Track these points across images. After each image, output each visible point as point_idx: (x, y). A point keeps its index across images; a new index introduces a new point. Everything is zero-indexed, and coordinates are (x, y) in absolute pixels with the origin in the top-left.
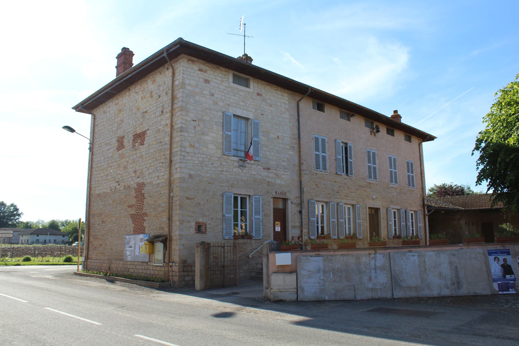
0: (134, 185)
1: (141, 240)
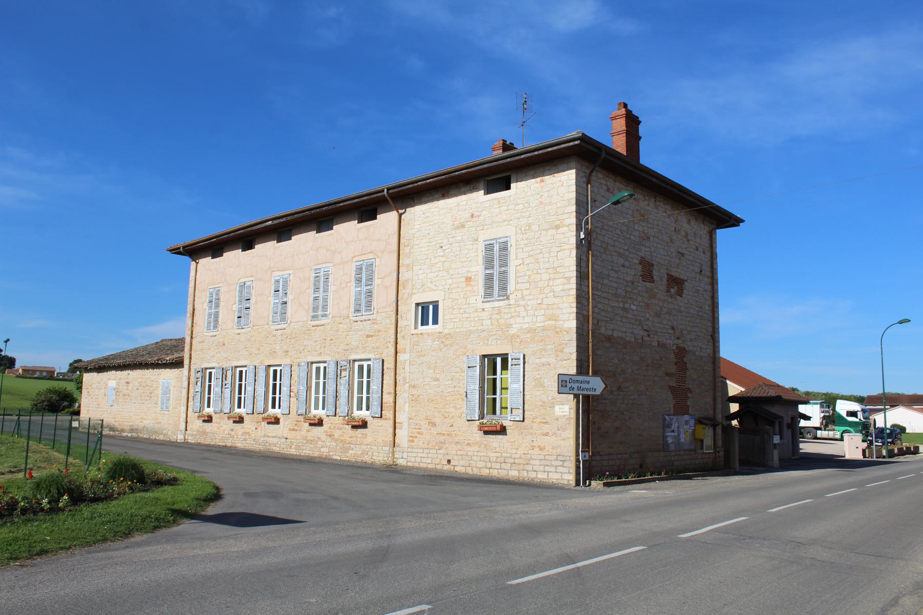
0: (672, 345)
1: (687, 422)
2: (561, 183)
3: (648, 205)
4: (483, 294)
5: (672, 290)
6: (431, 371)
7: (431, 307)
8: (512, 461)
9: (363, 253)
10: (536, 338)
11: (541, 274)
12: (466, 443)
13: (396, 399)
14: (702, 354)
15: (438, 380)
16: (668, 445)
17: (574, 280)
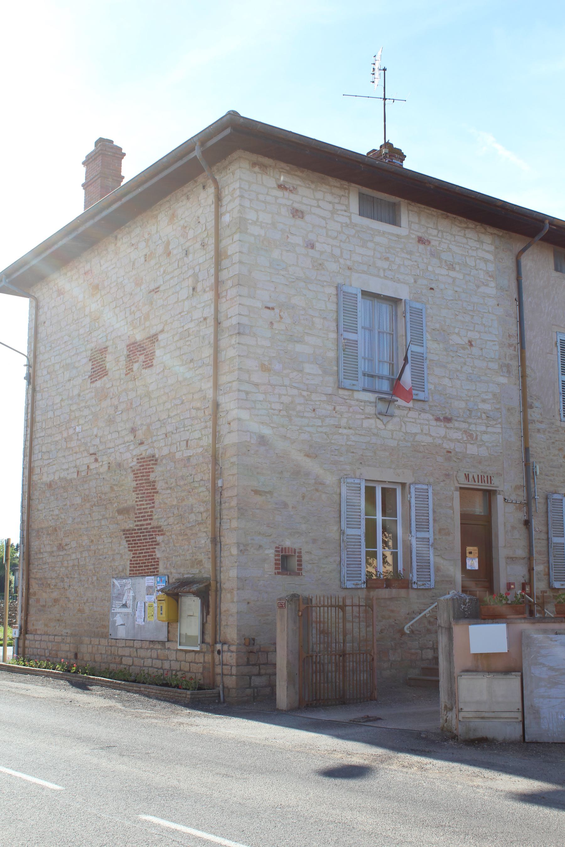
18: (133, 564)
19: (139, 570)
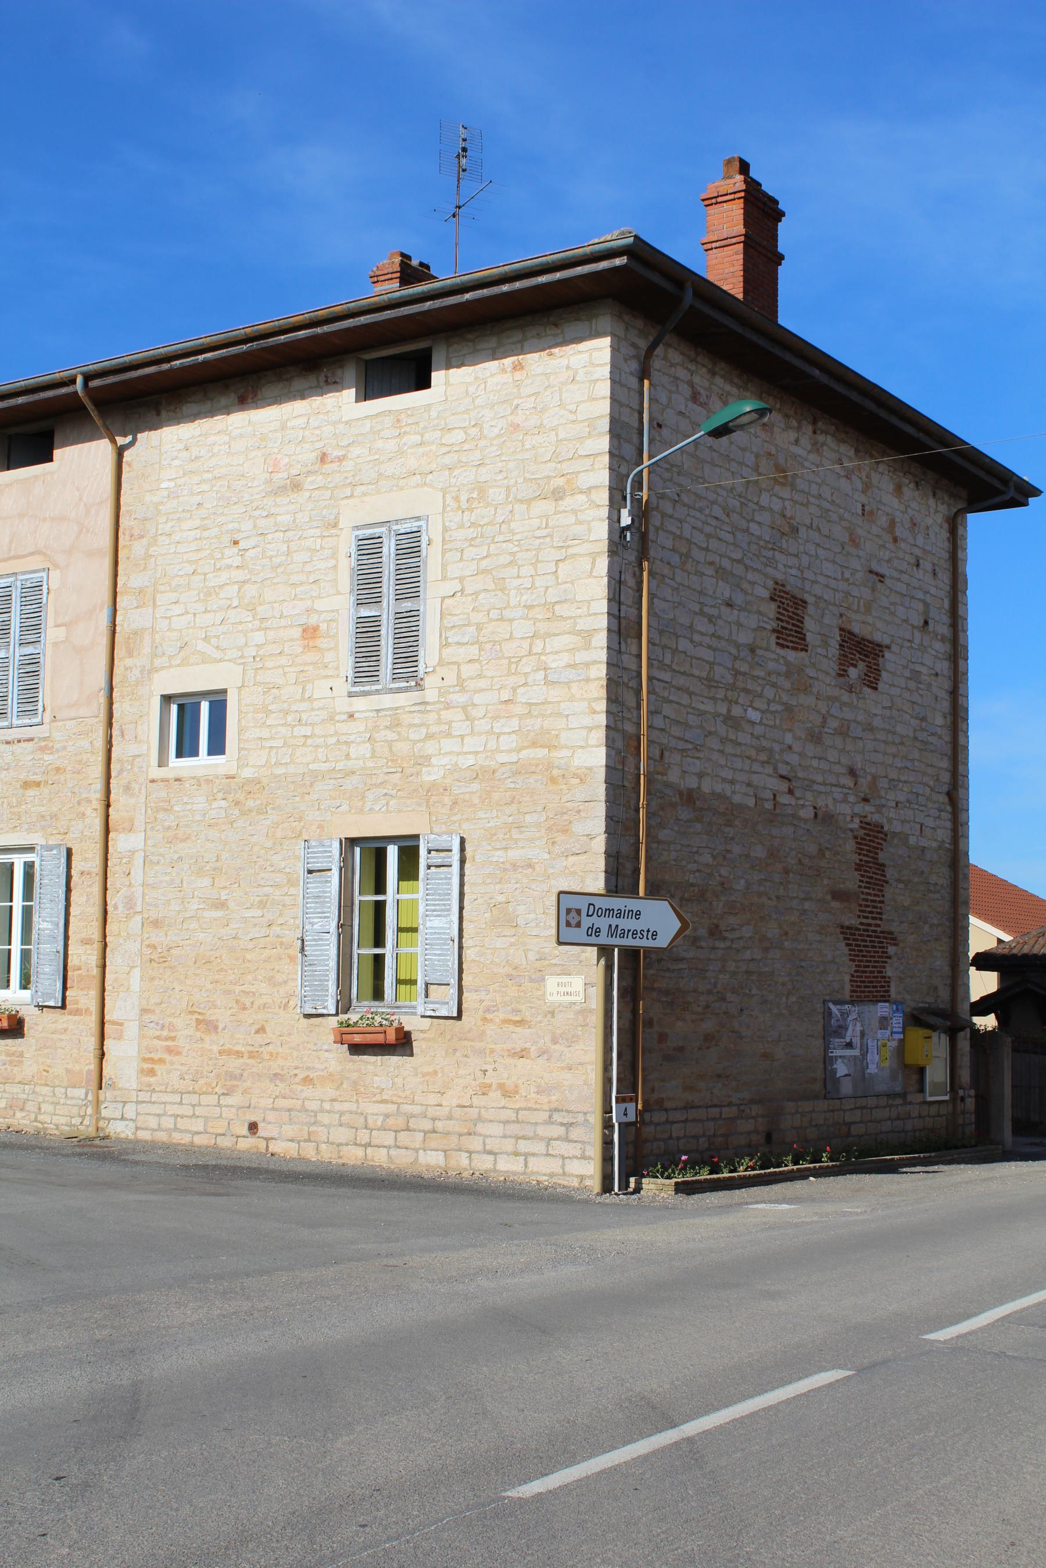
0: (848, 818)
2: (571, 373)
3: (797, 442)
4: (350, 674)
5: (853, 672)
6: (206, 881)
7: (205, 707)
8: (427, 1125)
9: (13, 553)
10: (496, 796)
11: (511, 621)
12: (301, 1076)
13: (104, 958)
14: (924, 843)
15: (222, 905)
16: (837, 1081)
17: (601, 639)
18: (856, 981)
19: (864, 992)
